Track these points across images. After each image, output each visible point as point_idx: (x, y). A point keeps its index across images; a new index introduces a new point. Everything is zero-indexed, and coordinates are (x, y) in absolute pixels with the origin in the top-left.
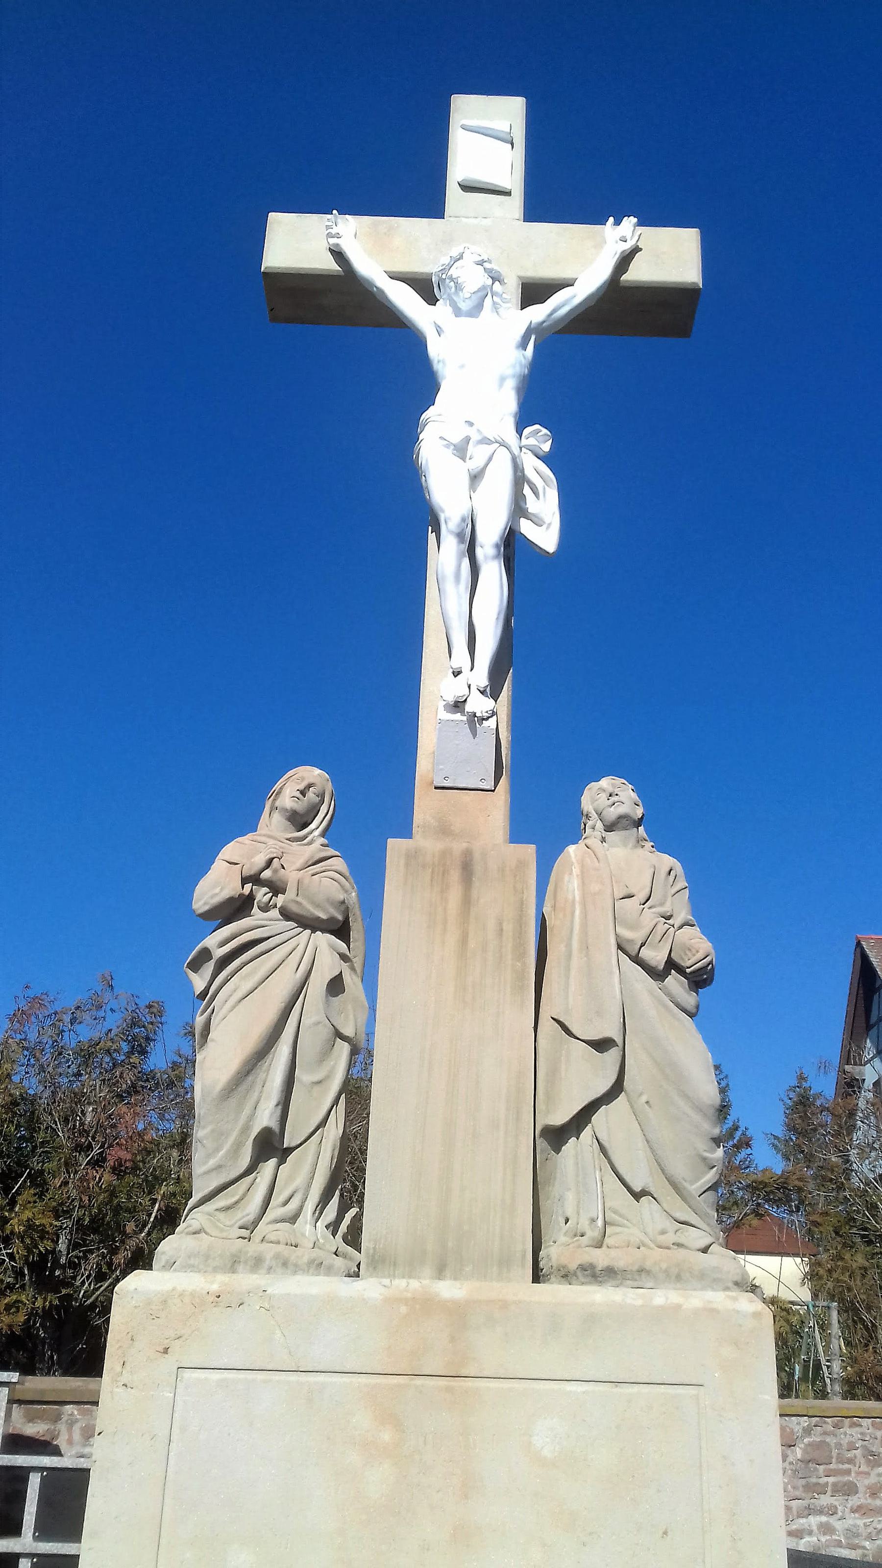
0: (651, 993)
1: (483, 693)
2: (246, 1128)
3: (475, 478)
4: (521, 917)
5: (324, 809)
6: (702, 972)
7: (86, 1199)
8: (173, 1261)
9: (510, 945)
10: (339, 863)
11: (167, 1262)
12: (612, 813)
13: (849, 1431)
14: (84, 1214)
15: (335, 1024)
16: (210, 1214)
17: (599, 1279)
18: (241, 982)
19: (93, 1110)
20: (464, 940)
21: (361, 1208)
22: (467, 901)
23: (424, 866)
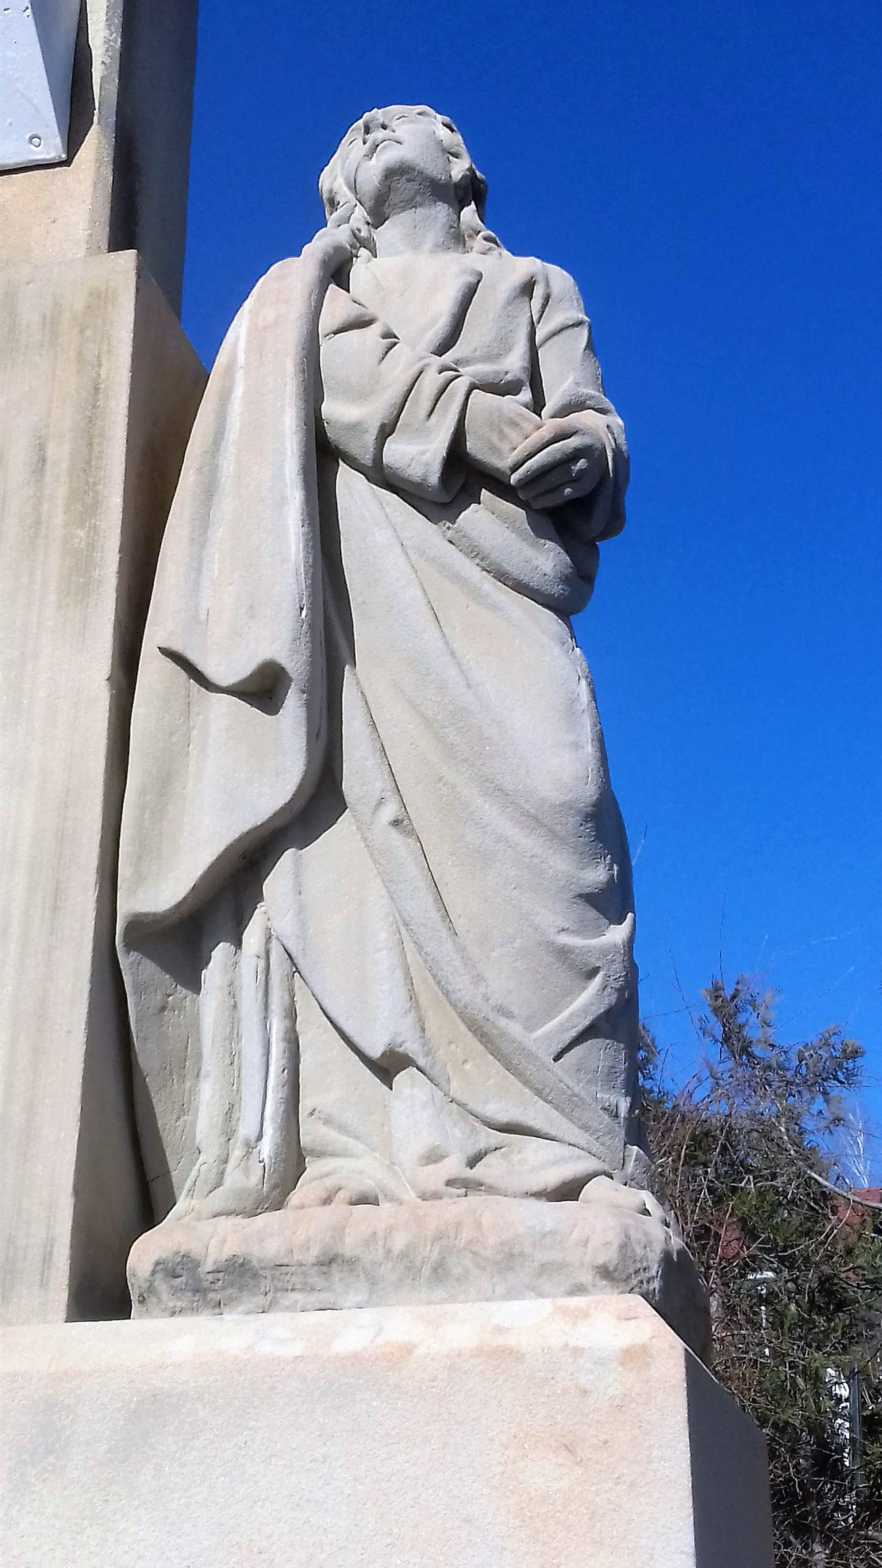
6: (553, 479)
9: (62, 491)
17: (212, 1295)
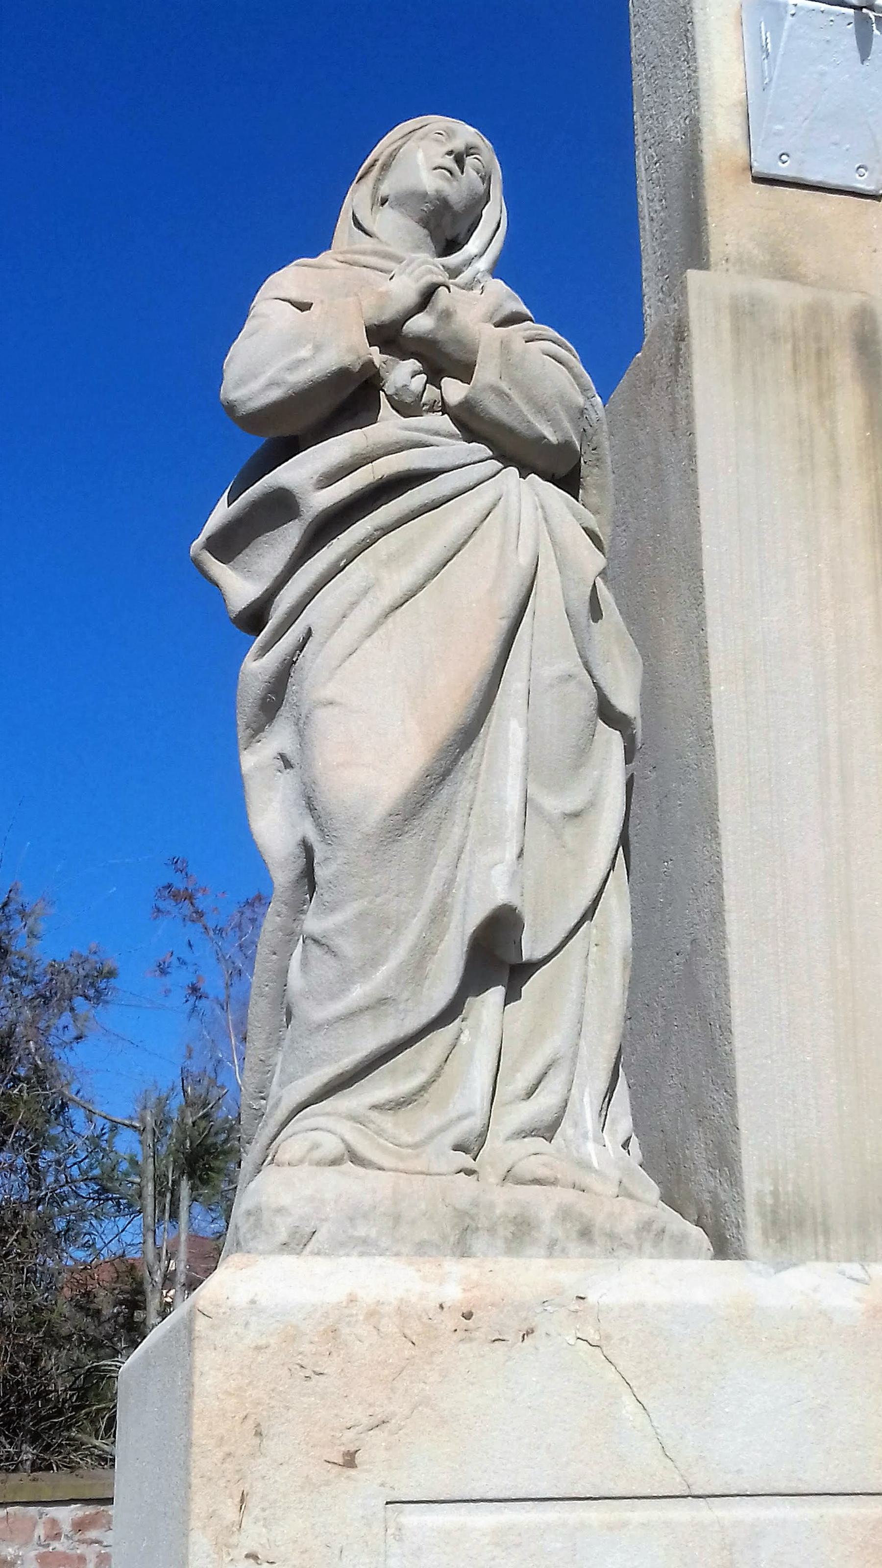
8: (309, 1230)
11: (294, 1232)
15: (602, 684)
23: (775, 336)
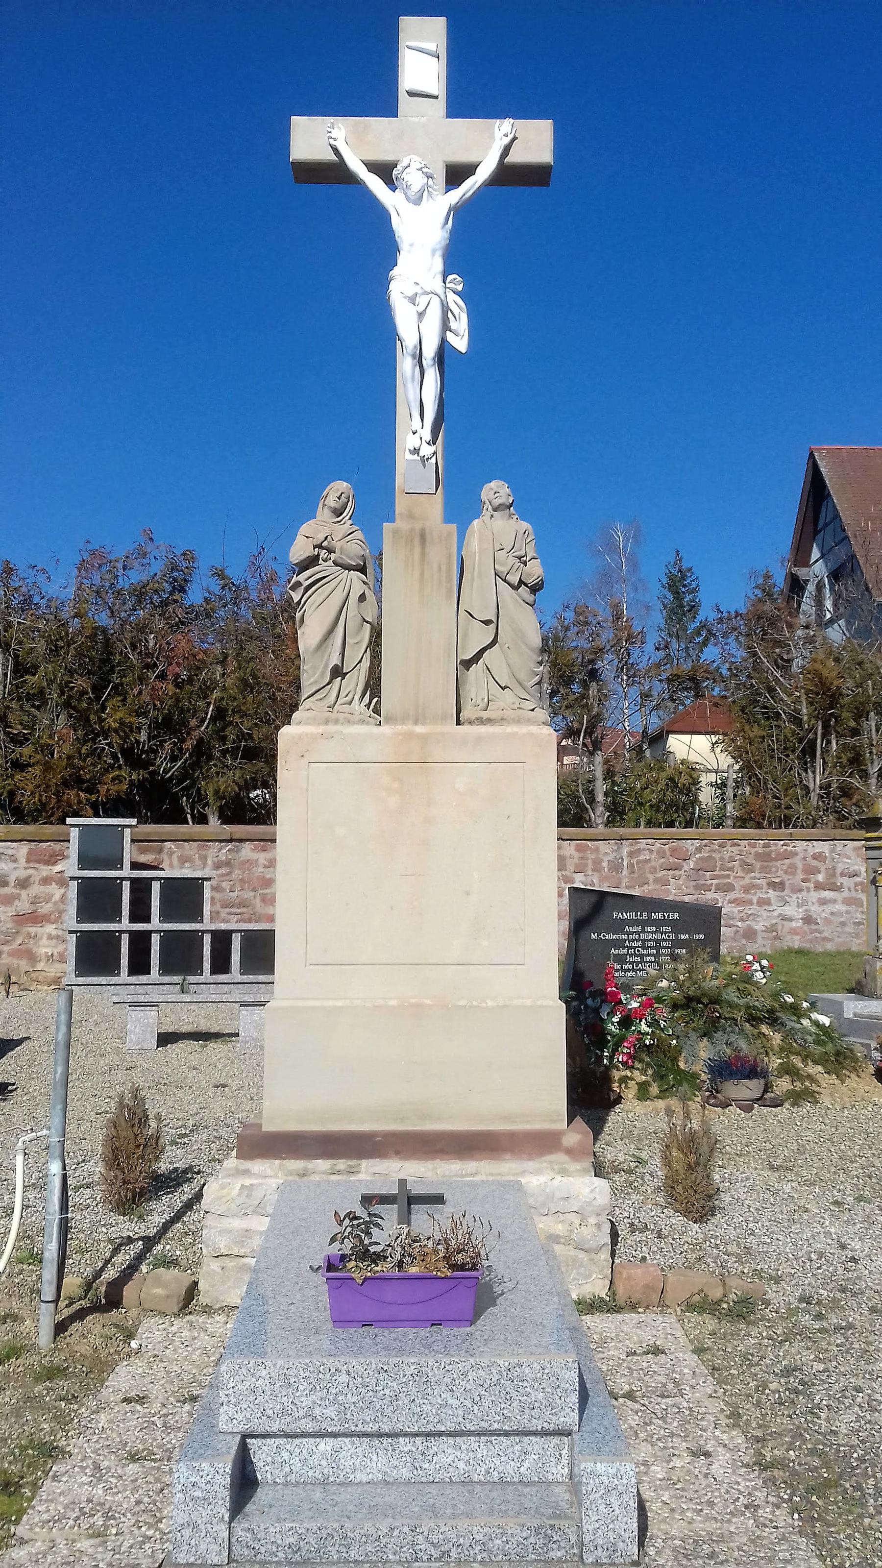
0: (512, 597)
1: (429, 444)
2: (326, 665)
3: (421, 315)
4: (449, 563)
5: (350, 504)
7: (157, 703)
10: (359, 535)
12: (496, 502)
13: (731, 849)
14: (158, 714)
16: (313, 702)
18: (317, 598)
19: (154, 638)
20: (422, 574)
21: (380, 697)
22: (423, 554)
